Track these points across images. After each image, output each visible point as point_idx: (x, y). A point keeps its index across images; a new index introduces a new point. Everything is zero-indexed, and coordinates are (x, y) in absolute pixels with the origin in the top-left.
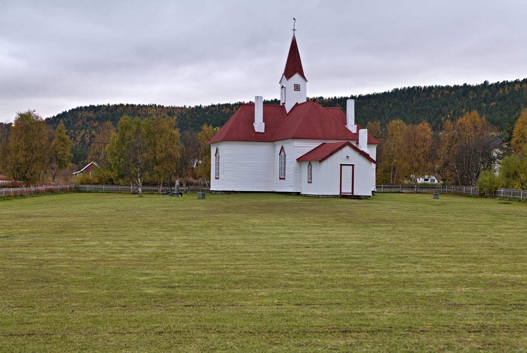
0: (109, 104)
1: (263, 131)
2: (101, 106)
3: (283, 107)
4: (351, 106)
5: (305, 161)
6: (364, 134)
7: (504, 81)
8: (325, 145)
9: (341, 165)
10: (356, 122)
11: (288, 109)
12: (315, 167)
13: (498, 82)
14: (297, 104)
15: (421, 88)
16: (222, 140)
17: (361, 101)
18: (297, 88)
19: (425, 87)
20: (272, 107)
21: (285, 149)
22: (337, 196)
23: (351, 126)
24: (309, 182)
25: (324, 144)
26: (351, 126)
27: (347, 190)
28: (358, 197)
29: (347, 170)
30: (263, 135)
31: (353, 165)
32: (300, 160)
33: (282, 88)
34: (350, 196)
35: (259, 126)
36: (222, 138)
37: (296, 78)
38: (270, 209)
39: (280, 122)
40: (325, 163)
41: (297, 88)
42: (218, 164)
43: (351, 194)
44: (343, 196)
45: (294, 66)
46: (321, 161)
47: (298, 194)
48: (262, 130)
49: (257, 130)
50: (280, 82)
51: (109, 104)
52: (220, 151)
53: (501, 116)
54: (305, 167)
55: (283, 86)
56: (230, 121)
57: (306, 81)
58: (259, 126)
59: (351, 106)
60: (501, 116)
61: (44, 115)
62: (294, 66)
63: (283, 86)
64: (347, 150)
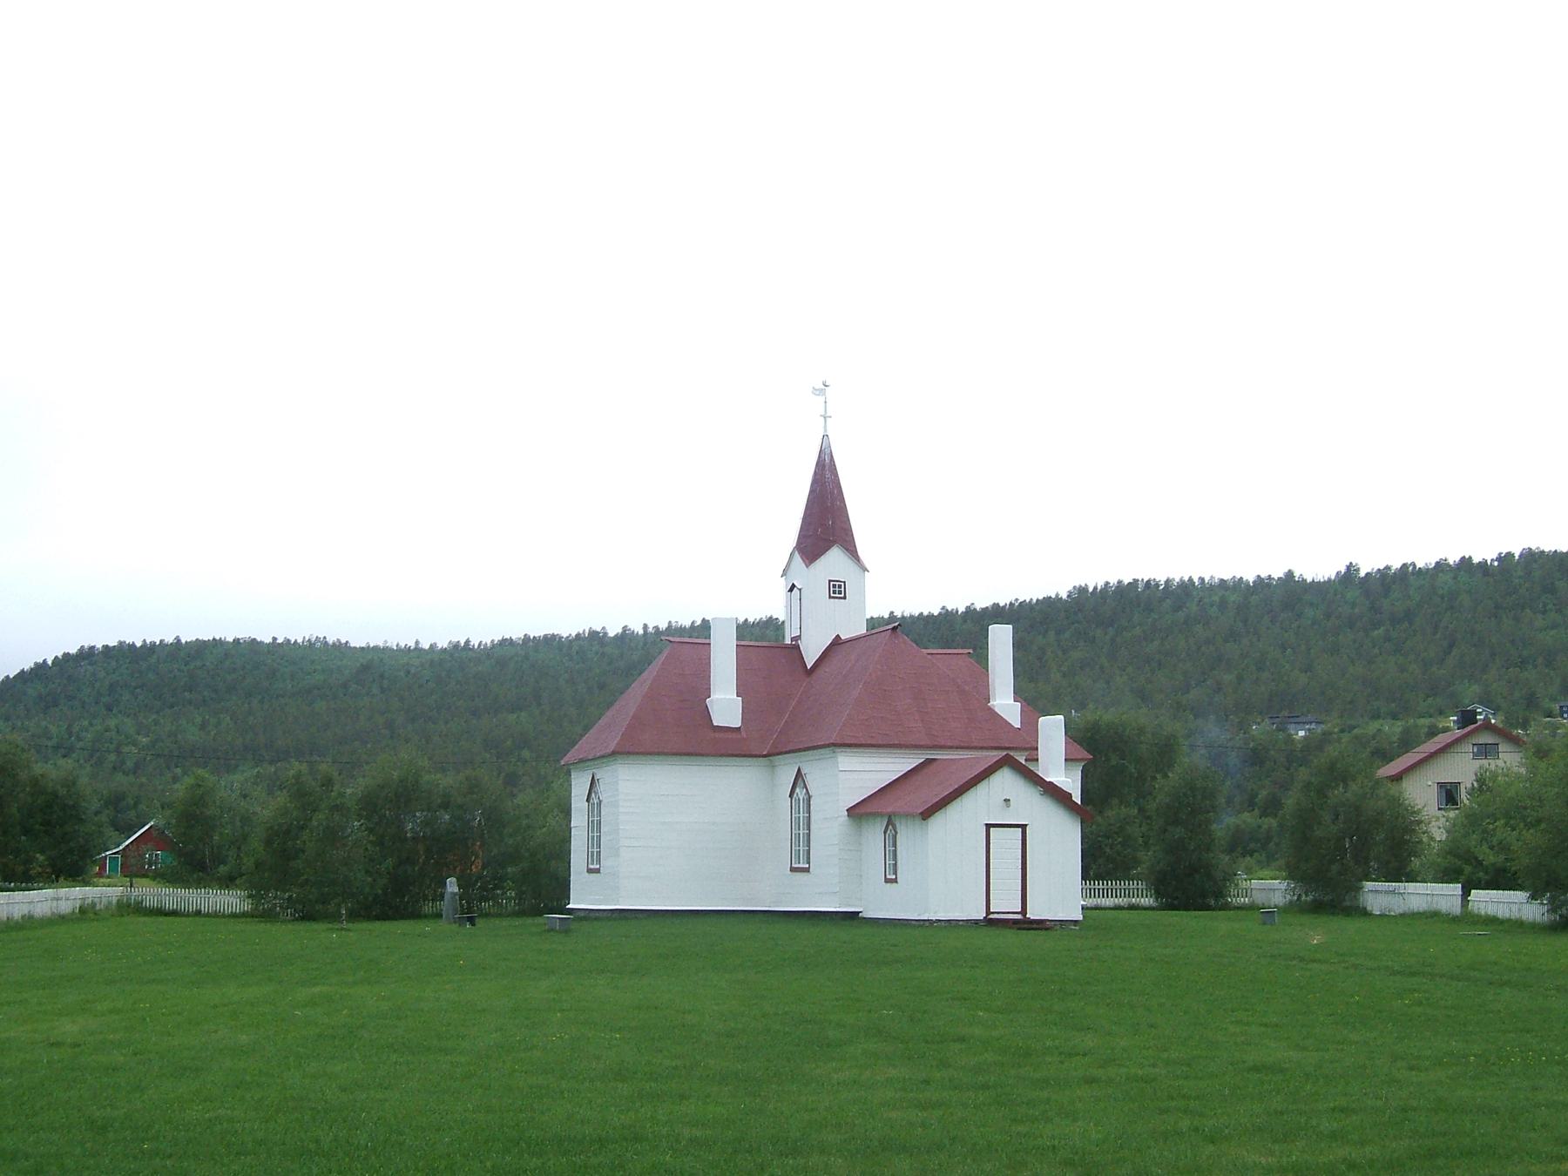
0: (178, 639)
1: (737, 723)
2: (153, 644)
3: (795, 649)
4: (1001, 638)
5: (875, 815)
6: (1052, 731)
7: (1404, 565)
8: (933, 767)
9: (988, 826)
10: (1018, 694)
11: (811, 656)
12: (907, 835)
13: (1388, 568)
14: (837, 641)
15: (1157, 585)
16: (614, 753)
17: (1037, 623)
18: (837, 590)
19: (1168, 581)
20: (764, 645)
21: (809, 780)
22: (976, 922)
23: (1005, 703)
24: (887, 881)
25: (928, 762)
26: (1005, 703)
27: (1006, 903)
28: (1040, 925)
29: (1005, 842)
30: (734, 736)
31: (1023, 827)
32: (859, 813)
33: (791, 590)
34: (1015, 922)
35: (725, 704)
36: (612, 747)
37: (833, 562)
38: (794, 839)
39: (796, 696)
40: (938, 820)
41: (837, 590)
42: (595, 826)
43: (1019, 917)
44: (990, 922)
45: (825, 525)
46: (927, 814)
47: (854, 915)
48: (735, 721)
49: (718, 720)
50: (784, 573)
51: (178, 639)
52: (604, 791)
53: (1402, 671)
54: (874, 835)
55: (793, 586)
56: (624, 691)
57: (865, 570)
58: (725, 704)
59: (1001, 638)
60: (1403, 670)
61: (1520, 896)
62: (825, 525)
63: (793, 586)
64: (1005, 783)
